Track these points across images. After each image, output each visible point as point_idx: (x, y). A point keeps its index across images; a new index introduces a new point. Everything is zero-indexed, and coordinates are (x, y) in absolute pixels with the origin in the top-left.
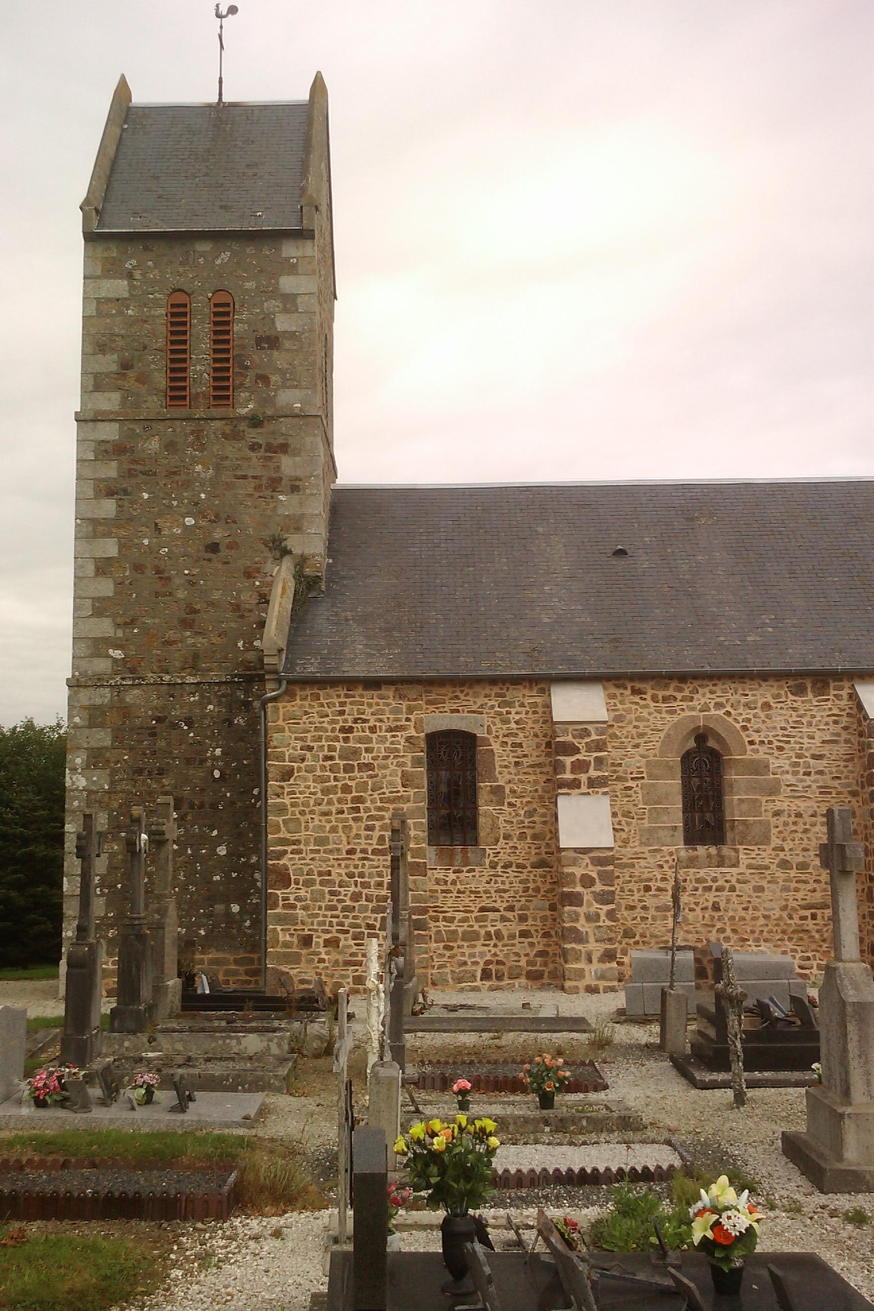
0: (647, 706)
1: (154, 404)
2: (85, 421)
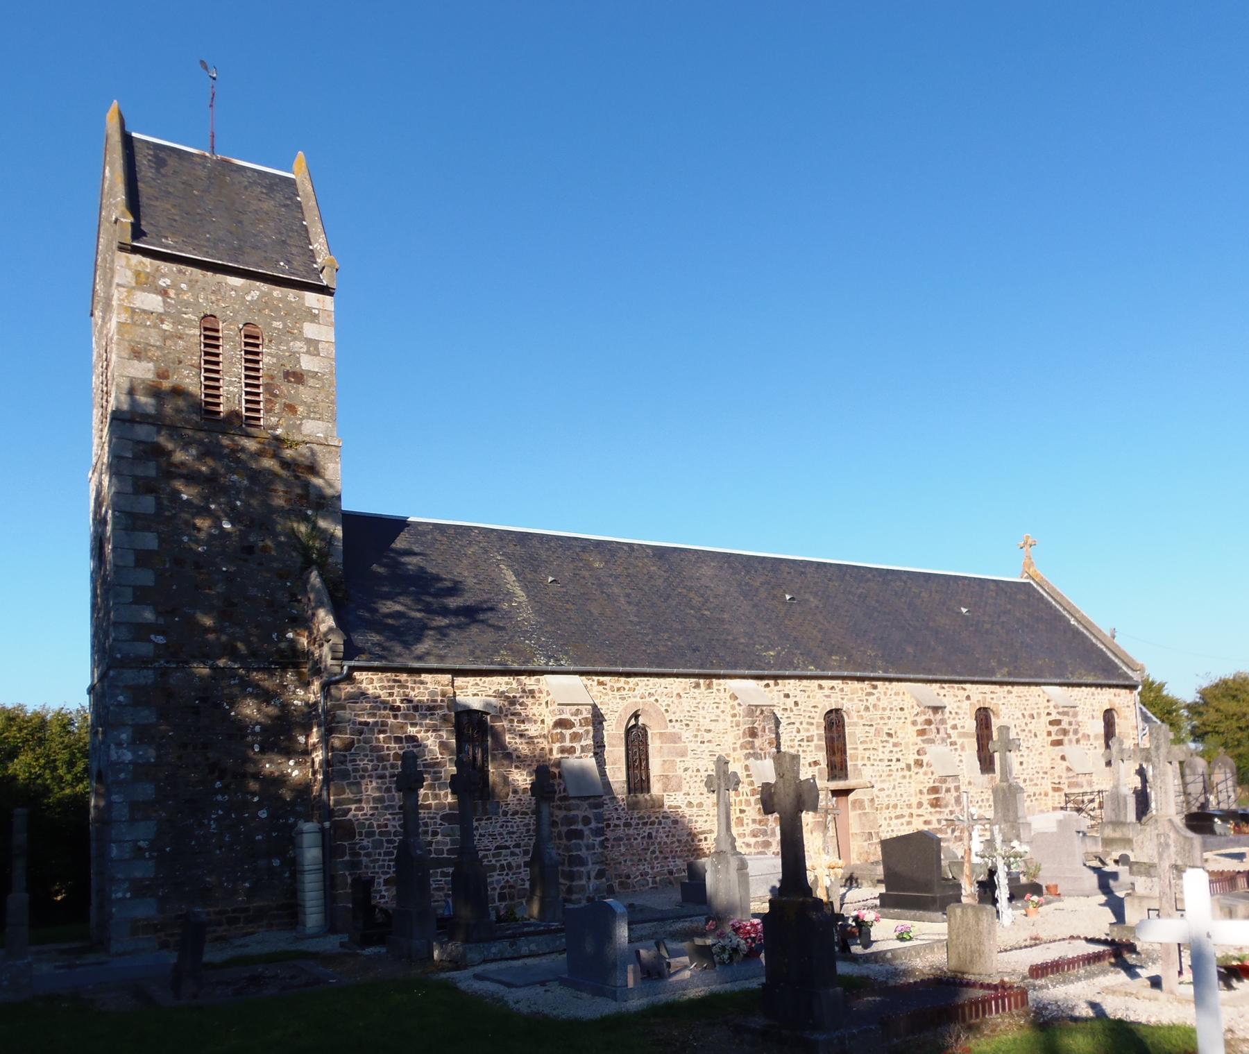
0: (606, 694)
2: (124, 421)
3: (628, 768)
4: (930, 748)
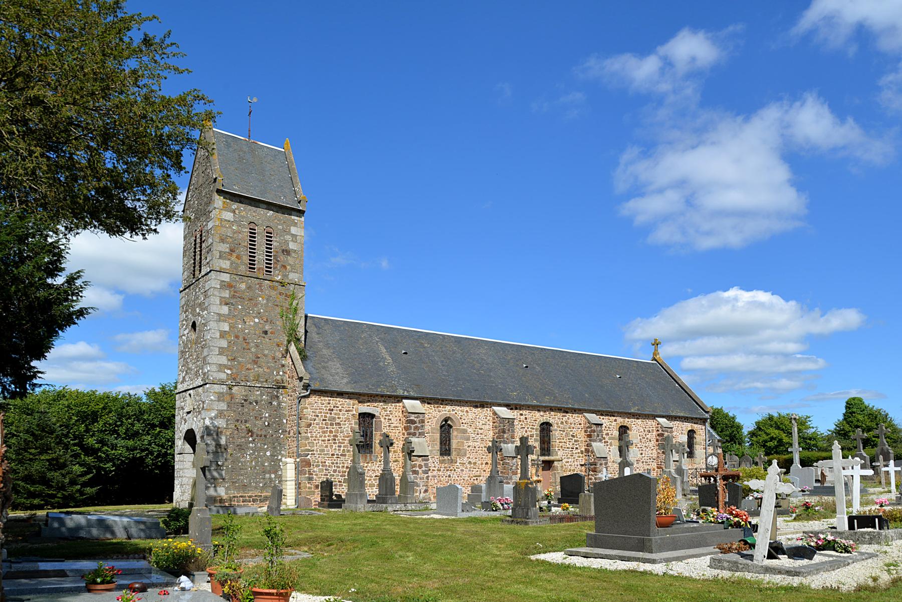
1: (243, 269)
3: (441, 443)
4: (594, 444)
